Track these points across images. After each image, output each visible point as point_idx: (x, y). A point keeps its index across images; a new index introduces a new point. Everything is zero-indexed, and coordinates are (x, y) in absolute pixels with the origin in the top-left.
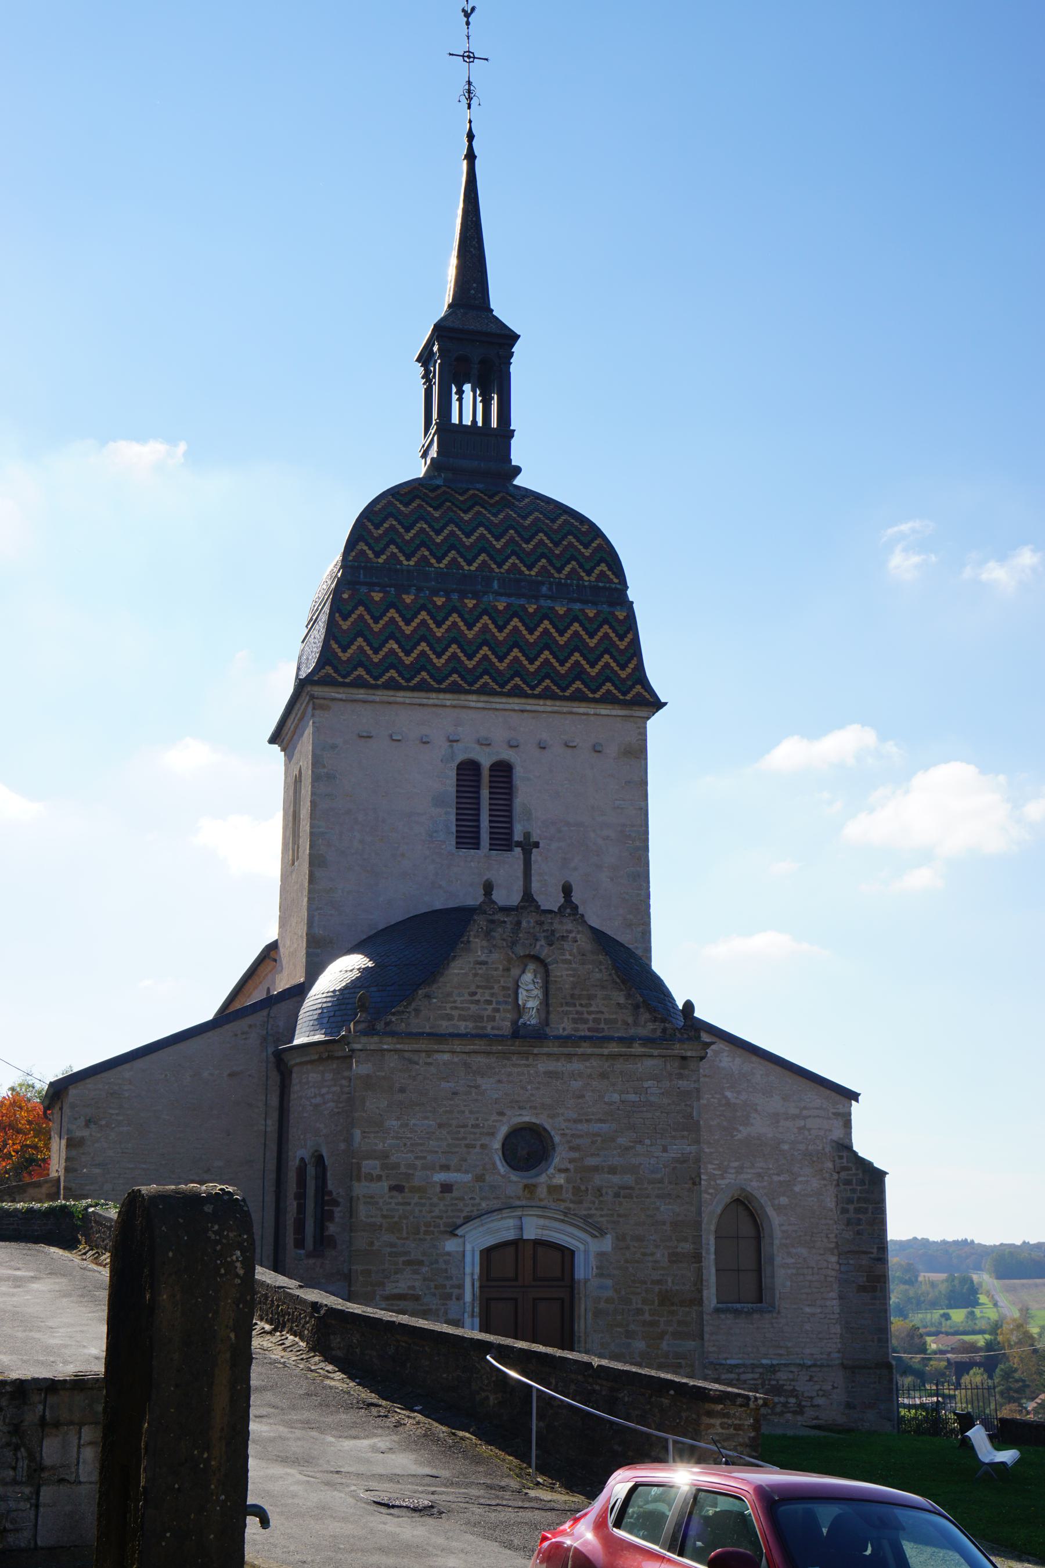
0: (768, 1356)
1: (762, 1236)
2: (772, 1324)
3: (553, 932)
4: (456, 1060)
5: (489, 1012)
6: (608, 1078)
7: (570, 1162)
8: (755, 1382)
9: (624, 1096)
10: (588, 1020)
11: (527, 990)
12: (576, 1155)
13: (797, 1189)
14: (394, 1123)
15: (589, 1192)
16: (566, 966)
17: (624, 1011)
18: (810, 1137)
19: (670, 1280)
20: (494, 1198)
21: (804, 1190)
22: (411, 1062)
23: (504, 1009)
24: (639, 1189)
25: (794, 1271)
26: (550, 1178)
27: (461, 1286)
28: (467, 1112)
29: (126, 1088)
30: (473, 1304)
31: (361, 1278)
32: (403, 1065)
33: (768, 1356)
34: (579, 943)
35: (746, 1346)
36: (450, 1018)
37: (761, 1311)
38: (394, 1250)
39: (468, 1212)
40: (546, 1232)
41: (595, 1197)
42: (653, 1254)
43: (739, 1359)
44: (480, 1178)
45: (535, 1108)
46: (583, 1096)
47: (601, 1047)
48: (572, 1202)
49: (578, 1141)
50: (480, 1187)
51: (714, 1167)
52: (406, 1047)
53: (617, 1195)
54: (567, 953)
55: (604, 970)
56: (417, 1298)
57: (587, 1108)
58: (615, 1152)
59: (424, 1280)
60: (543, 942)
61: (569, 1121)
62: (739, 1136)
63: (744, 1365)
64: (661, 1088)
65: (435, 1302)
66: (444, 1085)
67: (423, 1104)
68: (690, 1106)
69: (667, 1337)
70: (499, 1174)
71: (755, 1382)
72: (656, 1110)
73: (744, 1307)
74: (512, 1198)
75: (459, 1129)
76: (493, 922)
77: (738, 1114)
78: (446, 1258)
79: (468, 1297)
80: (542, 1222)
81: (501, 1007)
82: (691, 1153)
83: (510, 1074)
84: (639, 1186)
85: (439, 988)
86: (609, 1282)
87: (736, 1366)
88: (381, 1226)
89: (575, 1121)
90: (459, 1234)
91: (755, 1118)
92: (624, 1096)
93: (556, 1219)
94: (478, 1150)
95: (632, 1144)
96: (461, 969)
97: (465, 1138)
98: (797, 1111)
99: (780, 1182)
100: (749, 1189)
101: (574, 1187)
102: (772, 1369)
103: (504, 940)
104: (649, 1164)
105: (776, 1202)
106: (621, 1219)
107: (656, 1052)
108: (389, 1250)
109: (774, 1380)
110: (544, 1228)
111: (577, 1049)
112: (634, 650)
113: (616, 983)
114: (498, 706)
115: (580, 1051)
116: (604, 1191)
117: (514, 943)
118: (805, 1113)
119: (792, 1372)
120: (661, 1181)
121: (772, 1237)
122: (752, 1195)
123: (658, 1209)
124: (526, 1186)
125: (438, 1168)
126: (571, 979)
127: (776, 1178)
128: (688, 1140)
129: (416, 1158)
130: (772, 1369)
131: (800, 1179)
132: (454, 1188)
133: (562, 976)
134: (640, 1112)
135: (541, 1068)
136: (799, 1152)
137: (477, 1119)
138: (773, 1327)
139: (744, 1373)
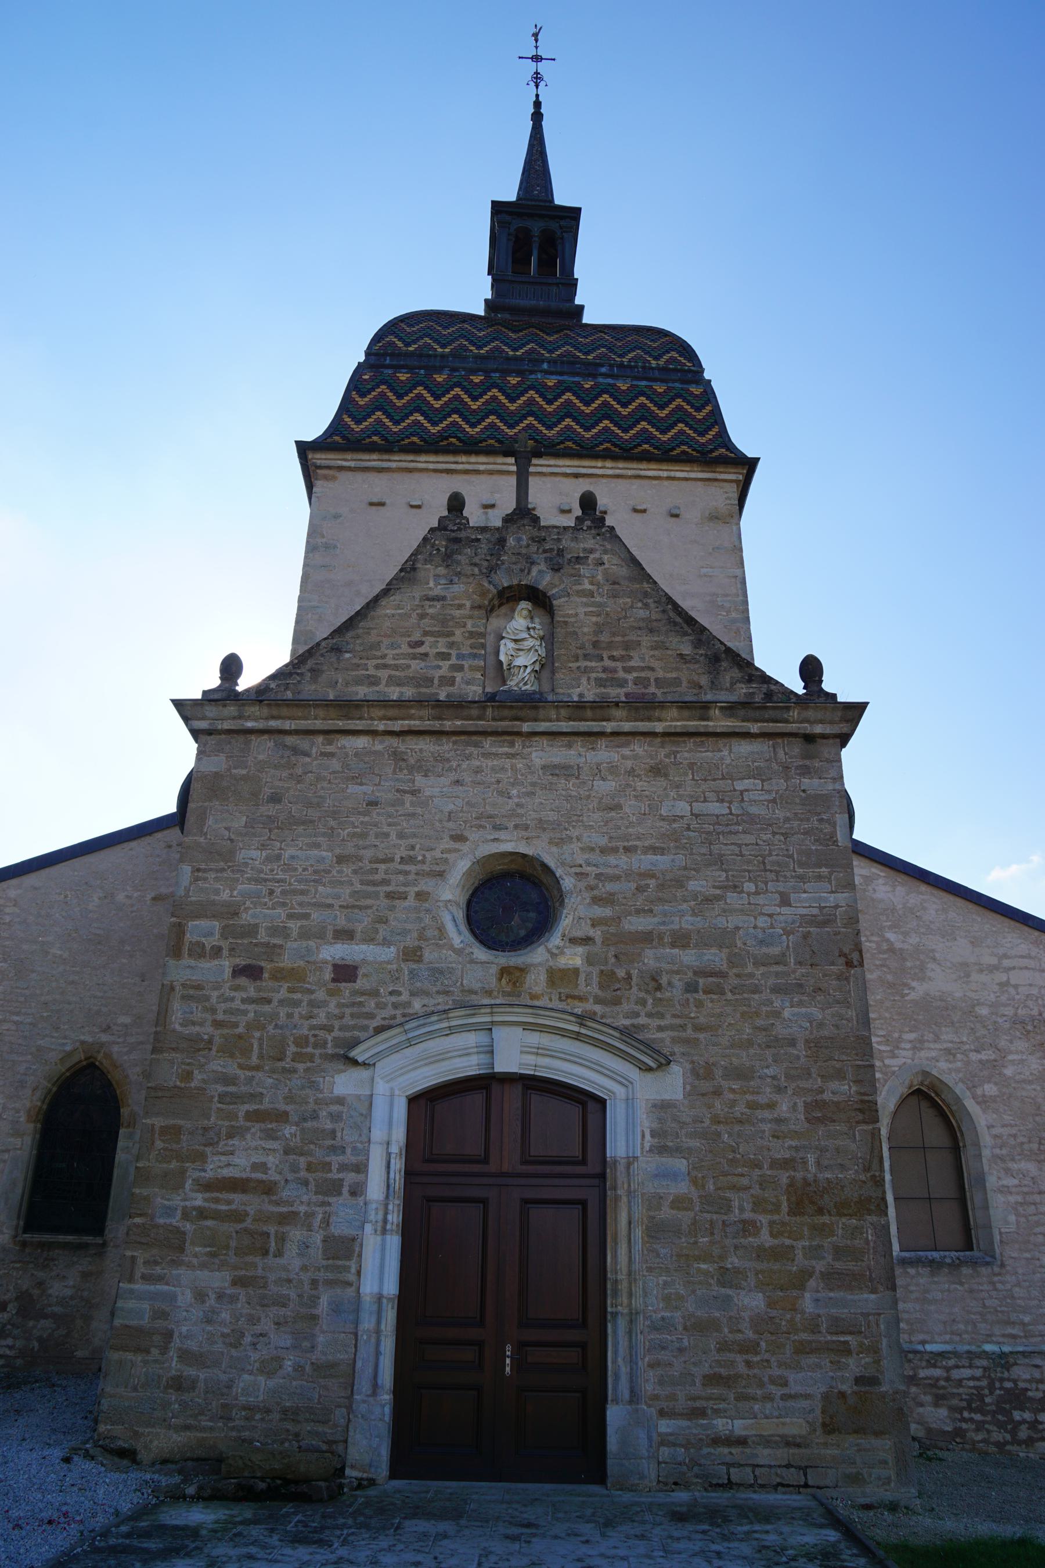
0: (994, 1339)
1: (961, 1144)
2: (993, 1283)
3: (561, 552)
4: (379, 747)
5: (444, 671)
6: (666, 775)
7: (593, 926)
8: (977, 1383)
9: (698, 807)
10: (626, 681)
11: (516, 641)
12: (607, 912)
13: (1009, 1072)
14: (255, 854)
15: (634, 982)
16: (584, 600)
17: (692, 666)
18: (1017, 997)
19: (811, 1159)
20: (438, 992)
21: (1020, 1073)
22: (296, 751)
23: (470, 666)
24: (738, 976)
25: (1020, 1199)
26: (554, 955)
27: (361, 1168)
28: (393, 836)
29: (7, 910)
30: (386, 1206)
31: (159, 1144)
32: (282, 757)
33: (994, 1339)
34: (606, 566)
35: (954, 1320)
36: (374, 681)
37: (974, 1263)
38: (231, 1089)
39: (384, 1019)
40: (546, 1061)
41: (647, 992)
42: (771, 1106)
43: (945, 1342)
44: (412, 955)
45: (526, 828)
46: (618, 807)
47: (649, 719)
48: (598, 1001)
49: (610, 887)
50: (411, 972)
51: (879, 1039)
52: (287, 725)
53: (691, 988)
54: (586, 581)
55: (652, 605)
56: (268, 1189)
57: (627, 827)
58: (685, 906)
59: (286, 1152)
60: (543, 567)
61: (592, 849)
62: (913, 996)
63: (955, 1354)
64: (769, 792)
65: (305, 1198)
66: (353, 789)
67: (312, 822)
68: (828, 821)
69: (812, 1283)
70: (452, 948)
71: (977, 1383)
72: (762, 829)
73: (945, 1257)
74: (476, 993)
75: (375, 866)
76: (457, 540)
77: (909, 964)
78: (335, 1108)
79: (375, 1190)
80: (534, 1039)
81: (466, 664)
82: (837, 907)
83: (478, 771)
84: (735, 970)
85: (358, 637)
86: (681, 1164)
87: (942, 1355)
88: (210, 1042)
89: (603, 851)
90: (360, 1060)
91: (933, 970)
92: (698, 807)
93: (562, 1033)
94: (411, 901)
95: (718, 892)
96: (398, 607)
97: (385, 882)
98: (994, 961)
99: (981, 1061)
100: (934, 1072)
101: (602, 972)
102: (1003, 1362)
103: (475, 565)
104: (755, 927)
105: (979, 1091)
106: (701, 1036)
107: (754, 728)
108: (221, 1088)
109: (1009, 1380)
110: (539, 1051)
111: (604, 723)
112: (716, 418)
113: (675, 624)
114: (544, 470)
115: (609, 727)
116: (664, 980)
117: (492, 569)
118: (1006, 963)
119: (1037, 1366)
120: (780, 960)
121: (977, 1145)
122: (941, 1081)
123: (777, 1014)
124: (504, 971)
125: (330, 935)
126: (594, 619)
127: (974, 1057)
128: (830, 882)
129: (290, 916)
130: (1003, 1362)
131: (1010, 1057)
132: (361, 972)
133: (577, 615)
134: (730, 833)
135: (538, 760)
136: (1005, 1018)
137: (413, 848)
138: (996, 1289)
139: (957, 1367)
